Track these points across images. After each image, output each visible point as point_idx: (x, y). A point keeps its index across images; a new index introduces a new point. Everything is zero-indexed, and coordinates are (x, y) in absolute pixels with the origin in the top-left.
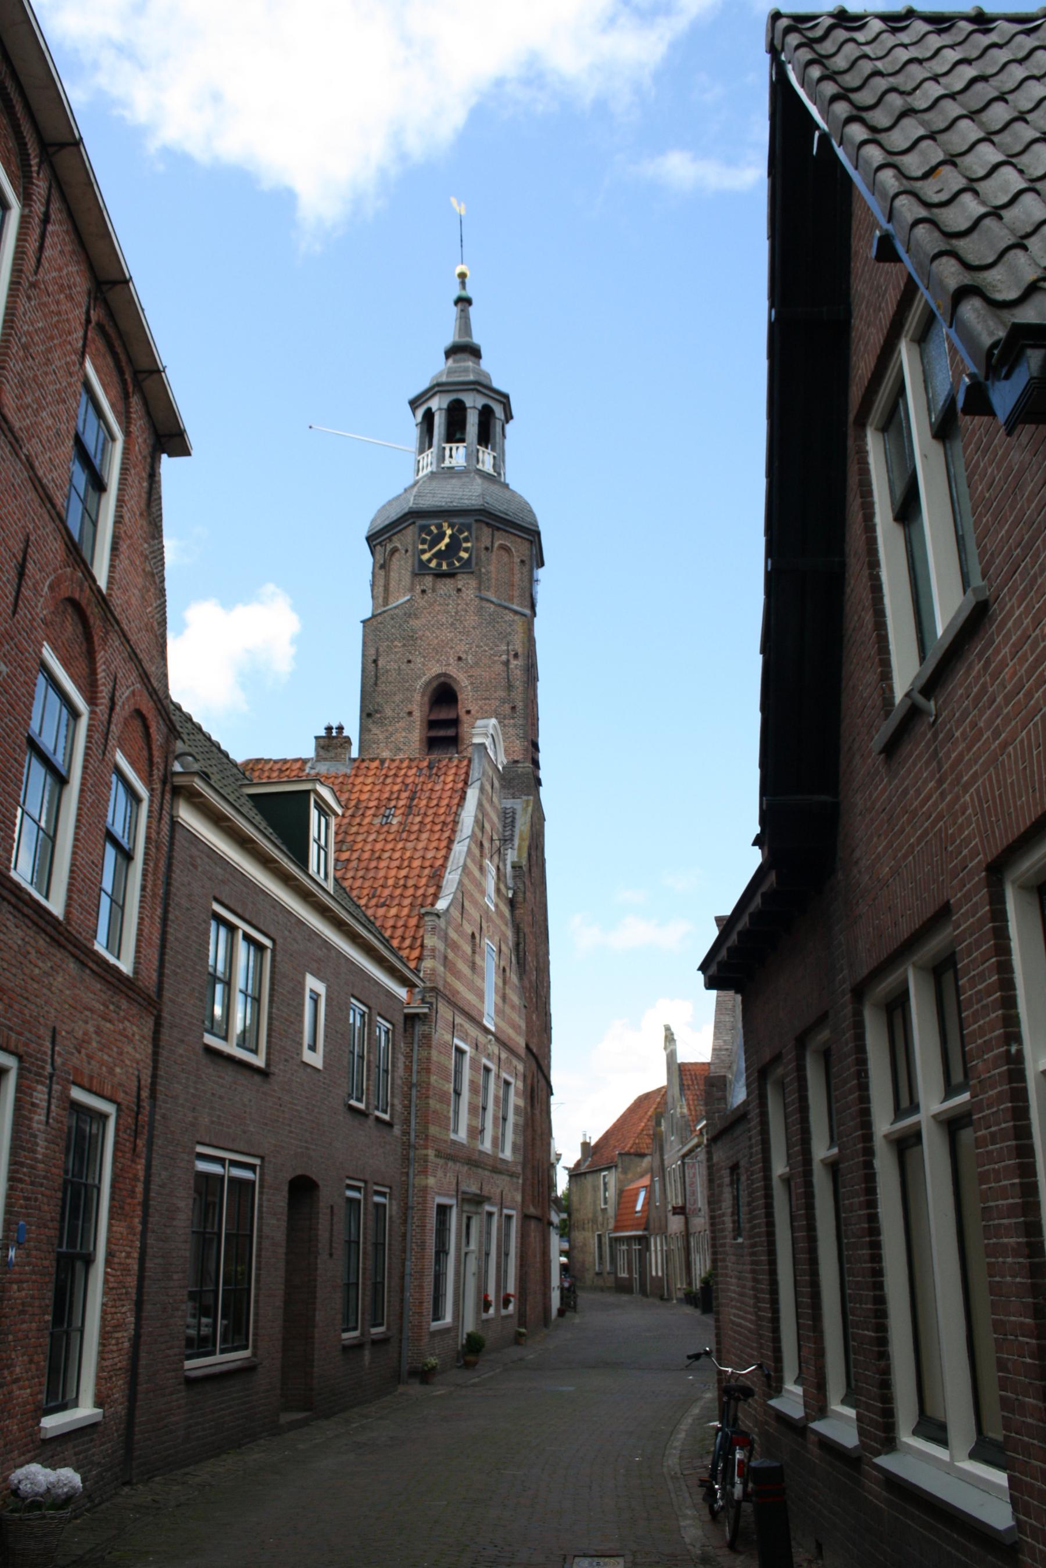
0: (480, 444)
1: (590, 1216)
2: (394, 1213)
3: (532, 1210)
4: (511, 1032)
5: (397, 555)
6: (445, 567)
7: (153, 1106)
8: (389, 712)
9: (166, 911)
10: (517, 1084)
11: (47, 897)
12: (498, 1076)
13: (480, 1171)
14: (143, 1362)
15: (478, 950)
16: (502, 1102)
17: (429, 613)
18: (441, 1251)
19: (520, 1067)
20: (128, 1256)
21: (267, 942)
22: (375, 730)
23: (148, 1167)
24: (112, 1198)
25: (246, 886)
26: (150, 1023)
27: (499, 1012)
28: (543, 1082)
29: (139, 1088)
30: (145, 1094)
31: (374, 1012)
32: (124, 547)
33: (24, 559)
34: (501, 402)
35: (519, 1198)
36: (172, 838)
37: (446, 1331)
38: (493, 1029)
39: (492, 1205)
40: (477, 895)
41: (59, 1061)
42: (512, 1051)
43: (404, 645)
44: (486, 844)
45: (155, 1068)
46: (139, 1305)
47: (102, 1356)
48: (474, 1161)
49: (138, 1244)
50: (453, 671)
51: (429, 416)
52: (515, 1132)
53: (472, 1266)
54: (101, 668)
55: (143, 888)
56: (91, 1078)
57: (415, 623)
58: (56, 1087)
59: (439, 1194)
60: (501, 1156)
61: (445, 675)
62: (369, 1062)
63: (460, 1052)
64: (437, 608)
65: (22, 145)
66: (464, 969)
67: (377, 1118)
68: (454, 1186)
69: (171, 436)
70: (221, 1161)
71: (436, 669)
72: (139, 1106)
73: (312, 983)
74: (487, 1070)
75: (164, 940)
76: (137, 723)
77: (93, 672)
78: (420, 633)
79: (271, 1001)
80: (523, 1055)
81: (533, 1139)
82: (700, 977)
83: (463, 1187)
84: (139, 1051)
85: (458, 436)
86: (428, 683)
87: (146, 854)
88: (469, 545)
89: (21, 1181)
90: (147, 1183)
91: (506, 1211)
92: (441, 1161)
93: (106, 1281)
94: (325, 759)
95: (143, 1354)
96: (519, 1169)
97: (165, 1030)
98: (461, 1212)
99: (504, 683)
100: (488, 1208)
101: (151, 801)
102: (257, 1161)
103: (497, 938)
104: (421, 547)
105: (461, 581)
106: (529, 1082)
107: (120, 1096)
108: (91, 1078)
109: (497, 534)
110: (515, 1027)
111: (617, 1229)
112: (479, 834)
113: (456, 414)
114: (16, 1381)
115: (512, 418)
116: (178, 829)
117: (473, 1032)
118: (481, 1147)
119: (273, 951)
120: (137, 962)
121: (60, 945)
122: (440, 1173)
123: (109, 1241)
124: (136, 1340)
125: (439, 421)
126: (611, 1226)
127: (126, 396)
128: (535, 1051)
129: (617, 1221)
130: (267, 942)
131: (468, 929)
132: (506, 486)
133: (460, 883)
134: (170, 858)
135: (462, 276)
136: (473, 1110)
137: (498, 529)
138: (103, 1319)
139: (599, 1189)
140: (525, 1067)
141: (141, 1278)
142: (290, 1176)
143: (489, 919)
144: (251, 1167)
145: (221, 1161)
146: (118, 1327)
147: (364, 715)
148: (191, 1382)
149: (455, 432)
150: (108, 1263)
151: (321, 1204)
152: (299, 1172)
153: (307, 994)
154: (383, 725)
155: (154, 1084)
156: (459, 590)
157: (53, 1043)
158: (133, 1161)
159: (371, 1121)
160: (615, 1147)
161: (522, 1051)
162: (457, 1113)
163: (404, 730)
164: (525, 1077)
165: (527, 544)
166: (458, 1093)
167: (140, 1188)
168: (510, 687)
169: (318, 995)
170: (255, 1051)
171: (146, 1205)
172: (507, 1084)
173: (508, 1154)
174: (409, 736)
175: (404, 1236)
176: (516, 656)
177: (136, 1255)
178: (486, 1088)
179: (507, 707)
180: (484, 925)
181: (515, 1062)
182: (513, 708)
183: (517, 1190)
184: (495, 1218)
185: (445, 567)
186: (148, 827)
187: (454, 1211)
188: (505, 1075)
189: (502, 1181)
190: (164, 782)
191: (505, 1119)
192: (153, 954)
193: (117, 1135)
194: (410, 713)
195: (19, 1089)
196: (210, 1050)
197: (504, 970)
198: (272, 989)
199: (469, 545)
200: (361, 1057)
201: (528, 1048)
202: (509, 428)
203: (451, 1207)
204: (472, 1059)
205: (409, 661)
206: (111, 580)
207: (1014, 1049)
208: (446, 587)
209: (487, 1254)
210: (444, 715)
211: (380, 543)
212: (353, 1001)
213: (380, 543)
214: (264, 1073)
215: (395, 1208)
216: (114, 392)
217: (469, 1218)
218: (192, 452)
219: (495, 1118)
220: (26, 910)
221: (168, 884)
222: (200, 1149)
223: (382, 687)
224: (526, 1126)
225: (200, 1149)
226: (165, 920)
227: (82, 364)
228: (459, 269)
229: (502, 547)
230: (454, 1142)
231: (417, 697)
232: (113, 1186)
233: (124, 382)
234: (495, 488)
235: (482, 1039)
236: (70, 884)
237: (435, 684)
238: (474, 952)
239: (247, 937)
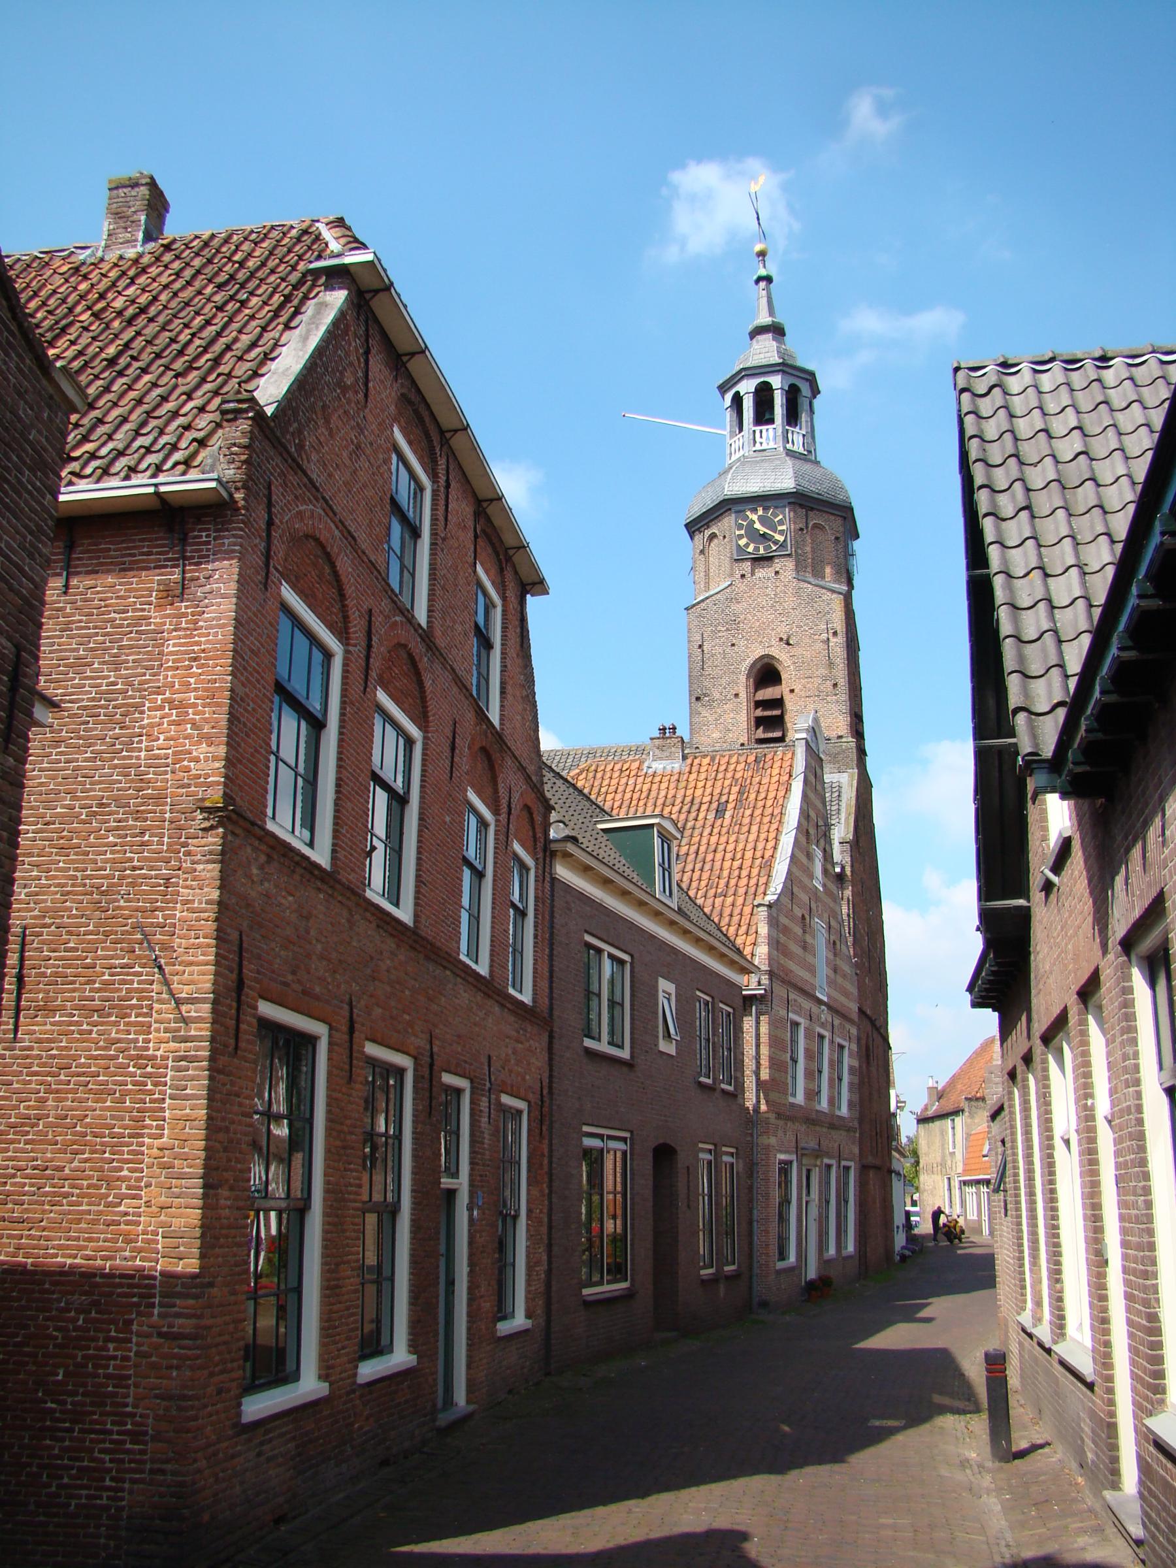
0: (789, 424)
1: (939, 1159)
2: (741, 1170)
3: (870, 1160)
4: (843, 999)
5: (716, 541)
6: (762, 551)
7: (551, 1099)
8: (716, 695)
9: (552, 950)
10: (850, 1047)
11: (477, 962)
12: (832, 1042)
13: (818, 1128)
14: (554, 1289)
15: (808, 929)
16: (836, 1064)
17: (750, 597)
18: (785, 1201)
19: (854, 1031)
20: (541, 1212)
21: (626, 957)
22: (704, 713)
23: (551, 1145)
24: (529, 1171)
25: (608, 916)
26: (545, 1037)
27: (831, 983)
28: (879, 1040)
29: (542, 1088)
30: (545, 1092)
31: (716, 1000)
32: (509, 689)
33: (454, 738)
34: (807, 380)
35: (856, 1150)
36: (552, 891)
37: (791, 1269)
38: (825, 999)
39: (830, 1157)
40: (805, 880)
41: (493, 1078)
42: (844, 1017)
43: (728, 630)
44: (812, 831)
45: (551, 1070)
46: (550, 1247)
47: (529, 1283)
48: (810, 1119)
49: (546, 1202)
50: (774, 652)
51: (738, 400)
52: (850, 1090)
53: (814, 1211)
54: (501, 786)
55: (536, 936)
56: (512, 1086)
57: (736, 608)
58: (493, 1096)
59: (781, 1152)
60: (837, 1113)
61: (768, 656)
62: (714, 1043)
63: (796, 1024)
64: (758, 591)
65: (430, 441)
66: (795, 949)
67: (723, 1090)
68: (793, 1144)
69: (534, 584)
70: (601, 1136)
71: (759, 652)
72: (542, 1101)
73: (665, 986)
74: (821, 1037)
75: (551, 972)
76: (525, 813)
77: (496, 791)
78: (742, 617)
79: (632, 1005)
80: (856, 1019)
81: (870, 1094)
82: (968, 997)
83: (802, 1144)
84: (539, 1061)
85: (767, 416)
86: (752, 666)
87: (535, 910)
88: (784, 527)
89: (477, 1164)
90: (551, 1156)
91: (843, 1163)
92: (781, 1123)
93: (528, 1230)
94: (661, 759)
95: (553, 1283)
96: (856, 1124)
97: (555, 1041)
98: (800, 1165)
99: (825, 660)
100: (826, 1161)
101: (537, 868)
102: (627, 1135)
103: (826, 915)
104: (738, 533)
105: (778, 564)
106: (863, 1042)
107: (531, 1096)
108: (512, 1086)
109: (811, 514)
110: (846, 994)
111: (966, 1171)
112: (805, 823)
113: (764, 395)
114: (482, 1297)
115: (819, 392)
116: (556, 884)
117: (806, 1004)
118: (818, 1108)
119: (632, 964)
120: (535, 993)
121: (489, 996)
122: (780, 1133)
123: (528, 1202)
124: (549, 1272)
125: (748, 404)
126: (960, 1170)
127: (502, 570)
128: (868, 1012)
129: (965, 1164)
130: (626, 957)
131: (798, 912)
132: (817, 463)
133: (789, 872)
134: (552, 906)
135: (762, 254)
136: (809, 1075)
137: (812, 509)
138: (528, 1256)
139: (947, 1133)
140: (859, 1029)
141: (550, 1227)
142: (653, 1144)
143: (817, 899)
144: (624, 1140)
145: (601, 1136)
146: (538, 1263)
147: (694, 699)
148: (588, 1304)
149: (763, 415)
150: (528, 1217)
151: (679, 1166)
152: (661, 1141)
153: (661, 994)
154: (711, 707)
155: (551, 1082)
156: (777, 573)
157: (489, 1066)
158: (540, 1142)
159: (717, 1094)
160: (962, 1091)
161: (855, 1016)
162: (794, 1078)
163: (732, 711)
164: (859, 1039)
165: (839, 521)
166: (795, 1061)
167: (546, 1161)
168: (831, 665)
169: (669, 994)
170: (621, 1047)
171: (550, 1174)
172: (841, 1047)
173: (844, 1111)
174: (734, 720)
175: (751, 1188)
176: (835, 634)
177: (545, 1211)
178: (821, 1053)
179: (829, 684)
180: (813, 906)
181: (848, 1026)
182: (835, 685)
183: (853, 1143)
184: (834, 1170)
185: (762, 551)
186: (536, 889)
187: (795, 1165)
188: (838, 1040)
189: (839, 1136)
190: (545, 851)
191: (840, 1080)
192: (545, 984)
193: (529, 1125)
194: (736, 695)
195: (472, 1102)
196: (589, 1052)
197: (834, 943)
198: (632, 995)
199: (784, 527)
200: (708, 1040)
201: (861, 1011)
202: (816, 402)
203: (791, 1162)
204: (806, 1029)
205: (733, 645)
206: (502, 718)
207: (1089, 1102)
208: (761, 573)
209: (828, 1202)
210: (768, 693)
211: (698, 529)
212: (698, 993)
213: (698, 529)
214: (629, 1065)
215: (741, 1166)
216: (493, 572)
217: (809, 1171)
218: (550, 591)
219: (831, 1080)
220: (470, 979)
221: (552, 927)
222: (586, 1129)
223: (708, 671)
224: (861, 1084)
225: (586, 1129)
226: (551, 956)
227: (475, 572)
228: (758, 247)
229: (816, 526)
230: (792, 1105)
231: (743, 678)
232: (528, 1162)
233: (500, 561)
234: (807, 467)
235: (815, 1009)
236: (492, 950)
237: (758, 666)
238: (804, 932)
239: (611, 956)
